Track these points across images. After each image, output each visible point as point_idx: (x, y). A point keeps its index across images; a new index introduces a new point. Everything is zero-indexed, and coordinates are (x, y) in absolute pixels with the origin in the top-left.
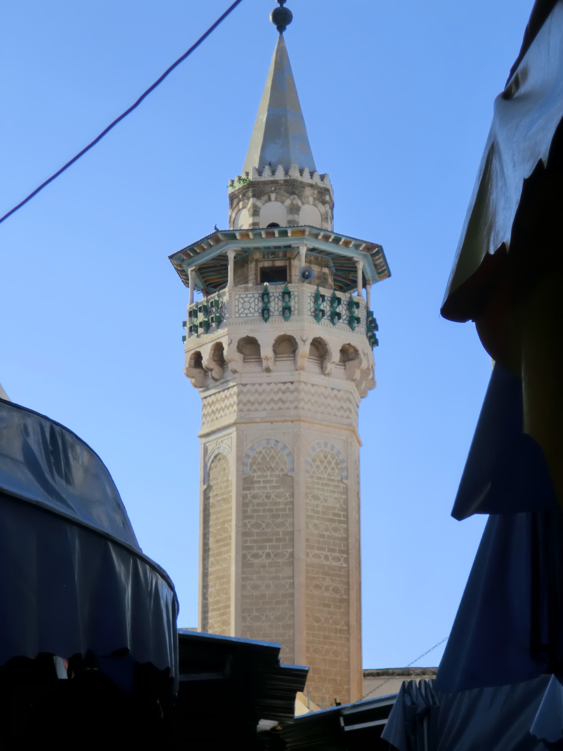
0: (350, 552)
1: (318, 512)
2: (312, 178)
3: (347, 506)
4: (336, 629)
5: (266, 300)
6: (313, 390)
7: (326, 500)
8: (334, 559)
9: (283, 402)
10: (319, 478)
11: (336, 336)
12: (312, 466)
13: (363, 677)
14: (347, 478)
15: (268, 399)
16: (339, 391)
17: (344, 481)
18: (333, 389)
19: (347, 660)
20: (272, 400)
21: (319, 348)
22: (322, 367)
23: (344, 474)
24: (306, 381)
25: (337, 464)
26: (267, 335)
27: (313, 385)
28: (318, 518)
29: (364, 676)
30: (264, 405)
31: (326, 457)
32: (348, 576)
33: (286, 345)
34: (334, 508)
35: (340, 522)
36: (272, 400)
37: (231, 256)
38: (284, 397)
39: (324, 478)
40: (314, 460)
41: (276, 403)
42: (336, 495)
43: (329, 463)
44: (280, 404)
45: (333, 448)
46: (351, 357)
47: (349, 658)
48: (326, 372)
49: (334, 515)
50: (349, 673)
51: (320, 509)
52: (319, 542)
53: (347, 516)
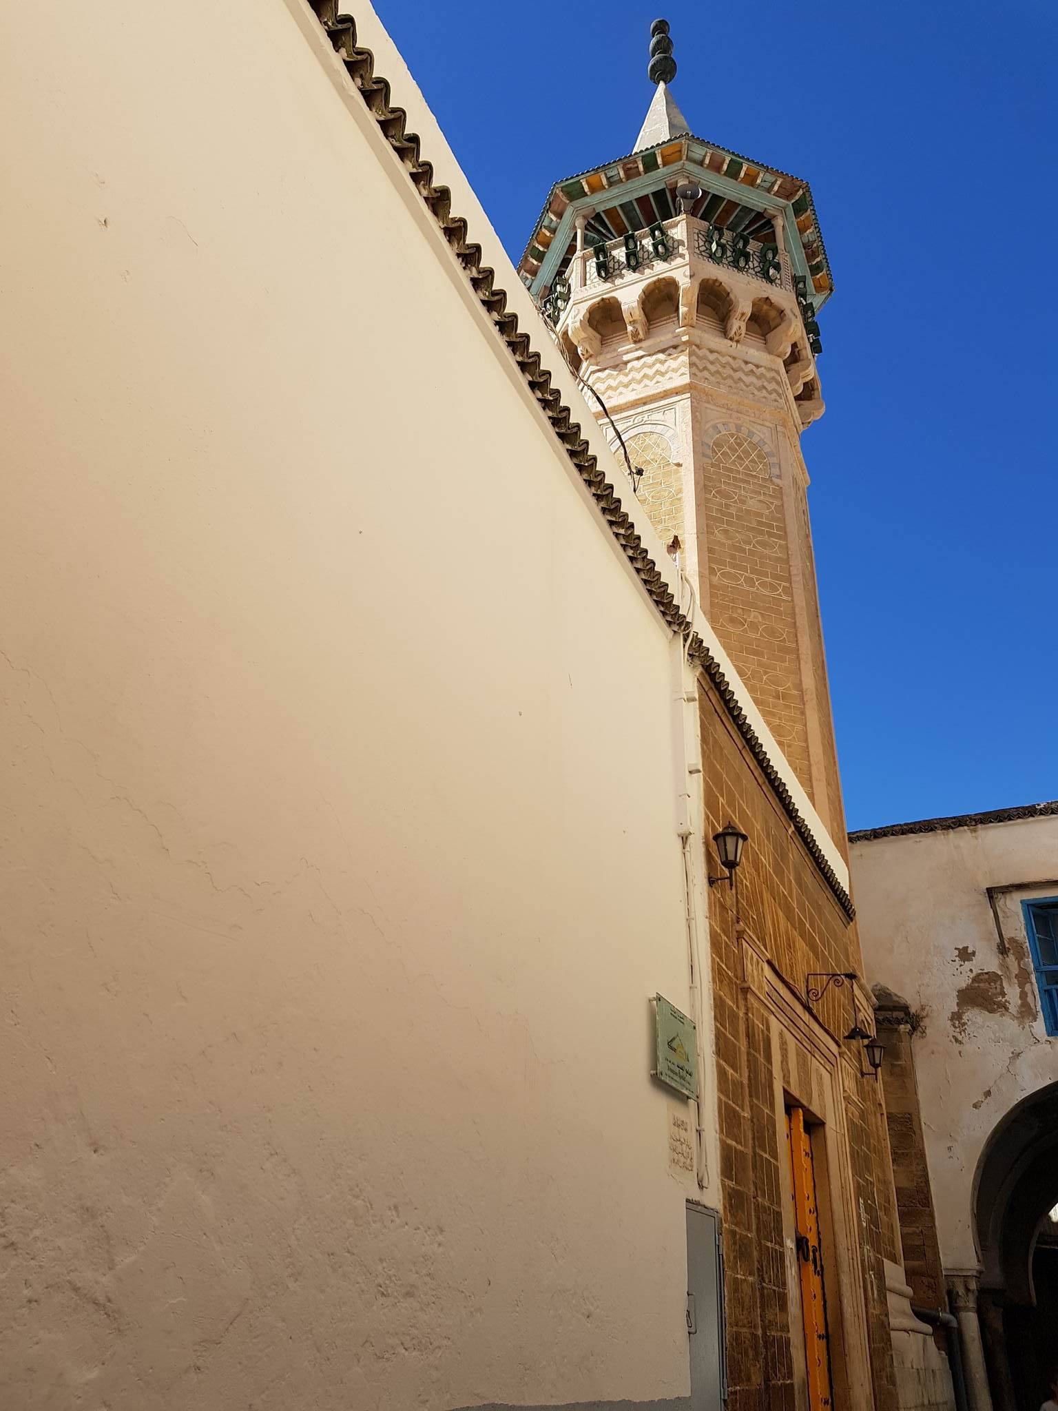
0: (793, 578)
1: (731, 515)
2: (676, 537)
3: (784, 515)
4: (777, 692)
5: (631, 246)
6: (712, 357)
7: (743, 502)
8: (763, 584)
9: (662, 374)
10: (731, 470)
11: (745, 288)
12: (714, 451)
13: (848, 844)
14: (779, 477)
15: (638, 376)
16: (758, 366)
17: (776, 480)
18: (746, 363)
19: (804, 744)
20: (645, 376)
21: (714, 301)
22: (725, 333)
23: (775, 471)
24: (698, 342)
25: (759, 456)
26: (629, 292)
27: (712, 351)
28: (728, 523)
29: (851, 840)
30: (633, 385)
31: (740, 445)
32: (794, 615)
33: (660, 300)
34: (761, 515)
35: (770, 535)
36: (645, 376)
37: (580, 223)
38: (663, 368)
39: (738, 472)
40: (718, 444)
41: (651, 378)
42: (762, 498)
43: (748, 454)
44: (658, 378)
45: (751, 434)
46: (773, 324)
47: (806, 741)
48: (732, 334)
49: (760, 523)
50: (810, 766)
51: (733, 511)
52: (733, 557)
53: (784, 530)
